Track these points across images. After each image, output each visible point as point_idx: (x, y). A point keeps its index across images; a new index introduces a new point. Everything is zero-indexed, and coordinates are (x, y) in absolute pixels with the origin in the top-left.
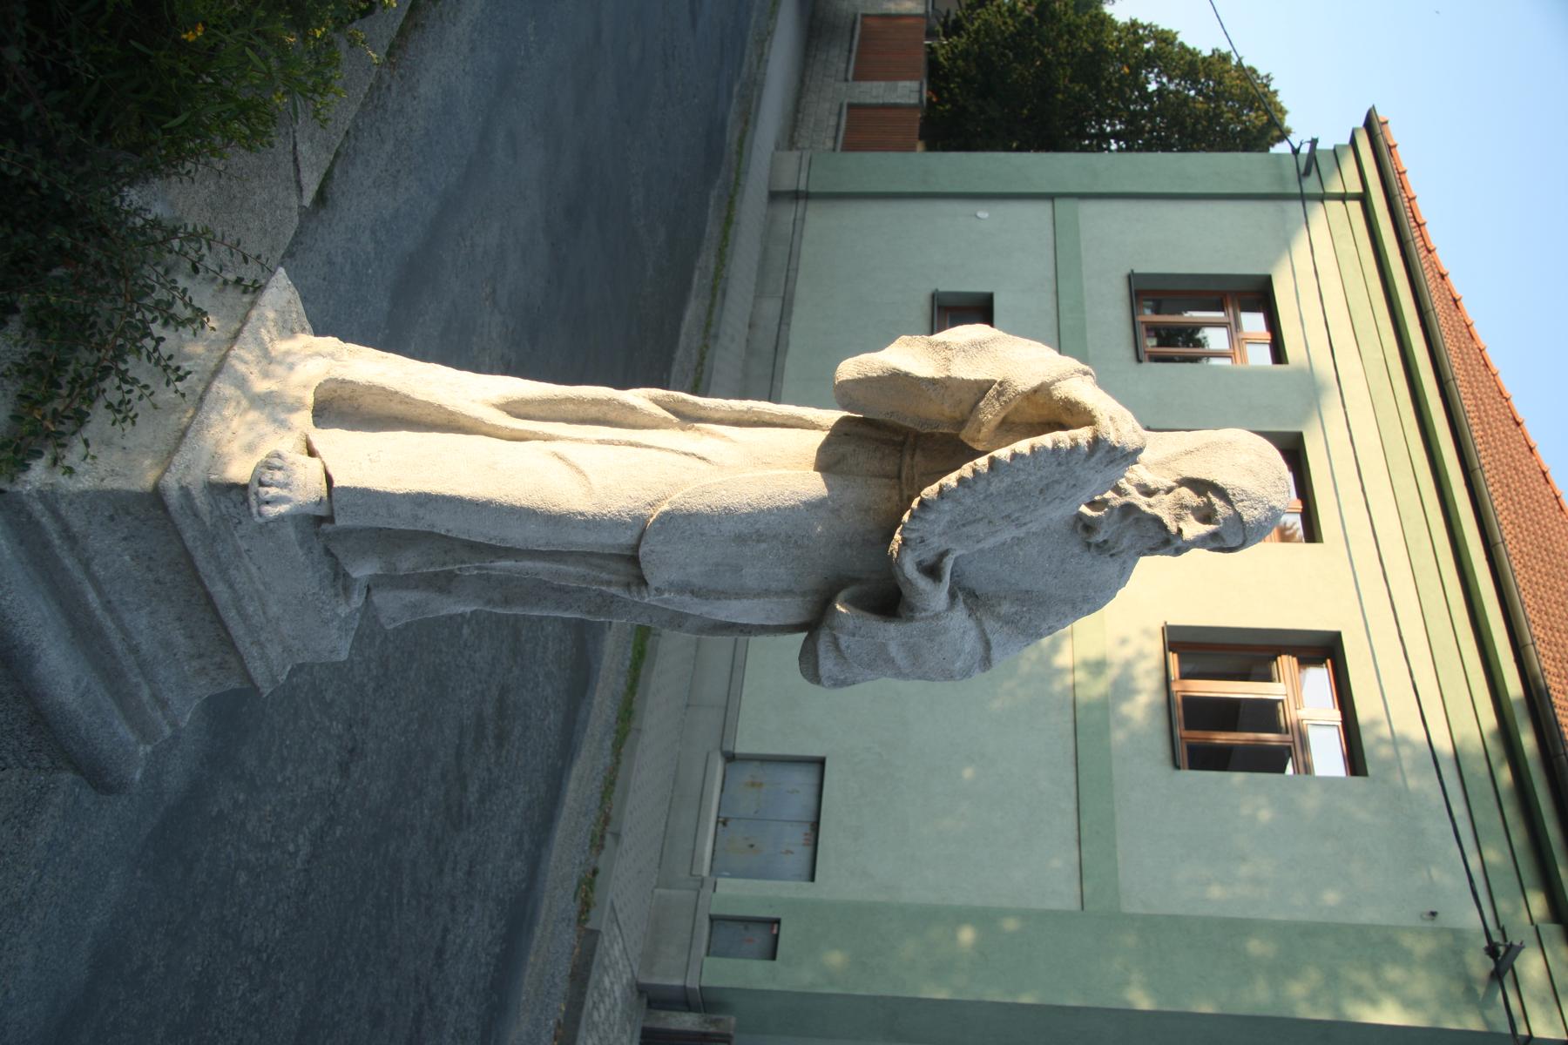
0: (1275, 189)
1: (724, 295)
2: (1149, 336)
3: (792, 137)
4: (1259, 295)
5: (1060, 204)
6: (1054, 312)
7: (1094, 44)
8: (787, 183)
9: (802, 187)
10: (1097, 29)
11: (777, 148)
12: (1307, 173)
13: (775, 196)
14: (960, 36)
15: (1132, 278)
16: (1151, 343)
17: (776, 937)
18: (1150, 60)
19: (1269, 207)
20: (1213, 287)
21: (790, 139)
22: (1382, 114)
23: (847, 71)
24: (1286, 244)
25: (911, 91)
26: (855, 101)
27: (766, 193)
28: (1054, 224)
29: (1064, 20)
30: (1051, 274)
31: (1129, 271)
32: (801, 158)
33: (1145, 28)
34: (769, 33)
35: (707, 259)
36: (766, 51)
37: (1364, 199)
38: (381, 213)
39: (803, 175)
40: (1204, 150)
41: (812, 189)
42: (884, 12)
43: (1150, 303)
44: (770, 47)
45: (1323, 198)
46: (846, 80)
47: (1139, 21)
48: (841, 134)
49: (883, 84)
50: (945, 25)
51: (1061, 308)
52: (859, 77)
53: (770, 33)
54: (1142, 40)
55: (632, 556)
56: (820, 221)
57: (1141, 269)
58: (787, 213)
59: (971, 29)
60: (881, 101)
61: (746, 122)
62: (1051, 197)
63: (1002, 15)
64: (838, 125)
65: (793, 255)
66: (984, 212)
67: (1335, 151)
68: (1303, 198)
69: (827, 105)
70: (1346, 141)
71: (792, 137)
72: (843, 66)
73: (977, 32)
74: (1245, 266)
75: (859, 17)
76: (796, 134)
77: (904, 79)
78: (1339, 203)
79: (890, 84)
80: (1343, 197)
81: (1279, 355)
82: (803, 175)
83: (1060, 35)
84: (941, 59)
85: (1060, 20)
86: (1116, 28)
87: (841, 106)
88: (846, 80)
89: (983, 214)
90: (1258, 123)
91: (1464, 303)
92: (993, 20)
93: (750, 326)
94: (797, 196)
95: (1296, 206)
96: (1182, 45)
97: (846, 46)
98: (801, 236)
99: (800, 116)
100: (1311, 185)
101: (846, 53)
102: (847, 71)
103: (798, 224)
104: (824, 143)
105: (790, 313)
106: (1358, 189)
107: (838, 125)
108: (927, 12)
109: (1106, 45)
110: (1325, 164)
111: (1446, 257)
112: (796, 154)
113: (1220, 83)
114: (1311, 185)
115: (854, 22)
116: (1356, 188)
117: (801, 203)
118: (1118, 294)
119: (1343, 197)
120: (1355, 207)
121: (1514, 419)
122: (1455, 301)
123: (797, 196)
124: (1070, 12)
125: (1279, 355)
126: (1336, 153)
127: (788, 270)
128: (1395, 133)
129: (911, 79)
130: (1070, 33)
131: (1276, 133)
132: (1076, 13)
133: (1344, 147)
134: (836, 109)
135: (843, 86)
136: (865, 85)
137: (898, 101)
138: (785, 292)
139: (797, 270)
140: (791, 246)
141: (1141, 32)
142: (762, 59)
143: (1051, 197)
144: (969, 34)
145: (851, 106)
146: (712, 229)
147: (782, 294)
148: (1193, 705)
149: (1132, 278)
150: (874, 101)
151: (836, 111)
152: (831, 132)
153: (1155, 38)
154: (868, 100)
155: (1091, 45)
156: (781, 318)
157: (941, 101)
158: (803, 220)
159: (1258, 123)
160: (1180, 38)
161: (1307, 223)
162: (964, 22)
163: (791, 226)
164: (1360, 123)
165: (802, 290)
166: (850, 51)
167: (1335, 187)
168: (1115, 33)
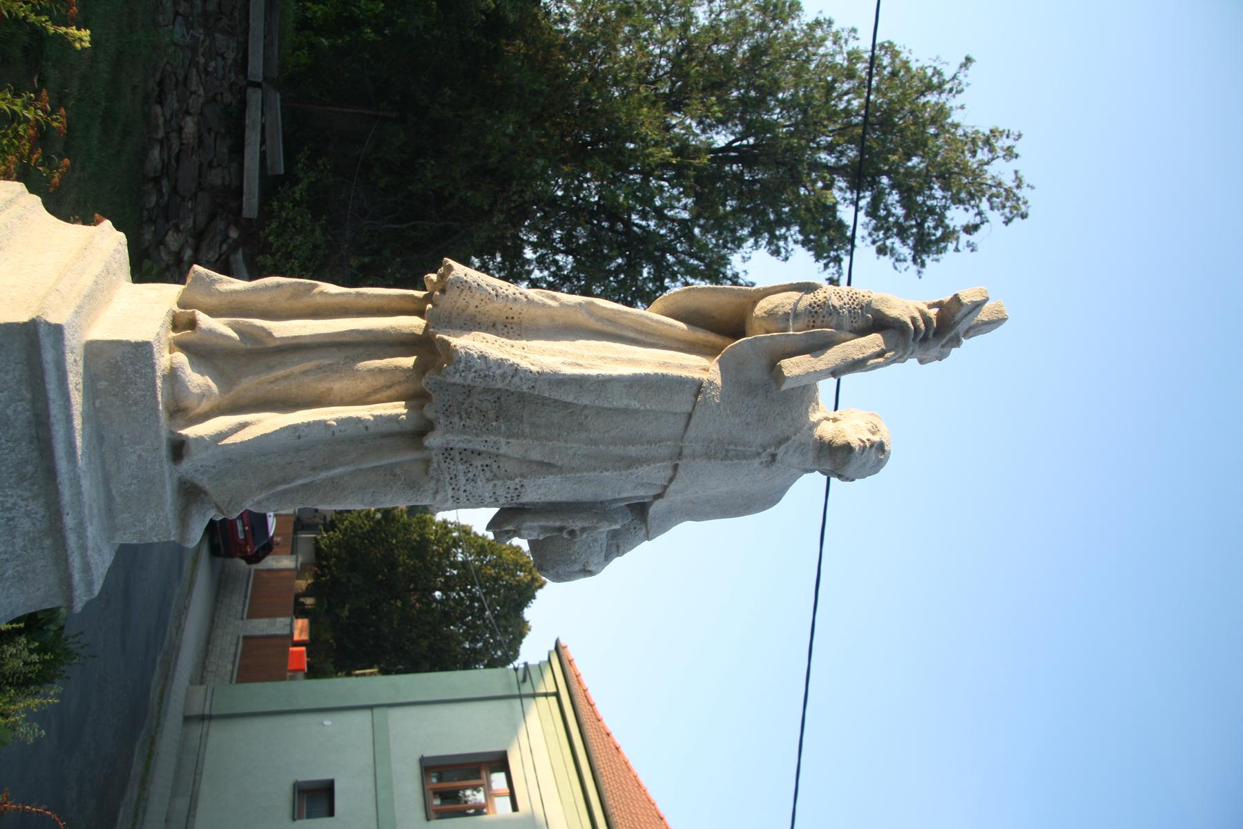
0: (507, 693)
1: (144, 812)
2: (435, 798)
3: (204, 663)
4: (500, 762)
5: (376, 711)
6: (373, 789)
7: (420, 535)
8: (196, 710)
9: (207, 712)
10: (422, 525)
11: (192, 683)
12: (524, 680)
13: (188, 719)
14: (335, 532)
15: (423, 760)
16: (437, 802)
18: (456, 543)
19: (504, 703)
20: (473, 760)
21: (201, 675)
22: (563, 642)
23: (243, 611)
24: (514, 731)
25: (285, 625)
26: (247, 634)
27: (181, 719)
28: (373, 726)
29: (401, 520)
30: (371, 762)
31: (419, 756)
32: (207, 690)
33: (452, 524)
34: (185, 608)
35: (132, 792)
36: (183, 623)
37: (557, 694)
38: (9, 167)
39: (208, 703)
40: (460, 669)
41: (214, 713)
42: (269, 567)
43: (436, 774)
44: (186, 618)
45: (534, 696)
46: (242, 619)
47: (448, 520)
48: (238, 660)
49: (266, 620)
50: (324, 525)
51: (378, 786)
52: (252, 615)
53: (186, 608)
54: (450, 531)
55: (230, 555)
56: (219, 734)
57: (428, 754)
58: (196, 730)
59: (342, 527)
60: (265, 633)
61: (166, 678)
62: (370, 707)
63: (361, 518)
64: (236, 653)
65: (199, 762)
66: (328, 721)
67: (539, 665)
68: (521, 697)
69: (229, 638)
70: (546, 659)
71: (204, 663)
72: (240, 608)
73: (346, 529)
74: (487, 745)
75: (252, 572)
76: (207, 661)
77: (280, 616)
78: (544, 698)
79: (272, 620)
80: (546, 695)
81: (515, 807)
82: (208, 703)
83: (398, 530)
84: (323, 547)
85: (398, 521)
86: (434, 524)
87: (238, 637)
88: (242, 619)
89: (327, 723)
90: (526, 580)
91: (623, 749)
92: (356, 522)
93: (167, 821)
94: (203, 718)
95: (517, 702)
96: (475, 534)
97: (243, 593)
98: (205, 748)
99: (210, 647)
100: (527, 689)
101: (243, 599)
102: (243, 611)
103: (204, 738)
104: (226, 667)
105: (196, 807)
106: (554, 690)
107: (236, 653)
108: (297, 567)
109: (427, 536)
110: (535, 674)
111: (610, 723)
112: (203, 687)
113: (500, 557)
114: (527, 689)
115: (249, 576)
116: (552, 689)
117: (206, 723)
118: (414, 770)
119: (546, 695)
120: (553, 699)
121: (659, 816)
122: (617, 749)
123: (203, 718)
124: (405, 516)
125: (515, 807)
126: (540, 667)
127: (195, 774)
128: (573, 652)
129: (285, 615)
130: (405, 529)
131: (537, 584)
132: (408, 516)
133: (544, 662)
134: (235, 641)
135: (240, 623)
136: (255, 622)
137: (277, 632)
138: (192, 792)
139: (201, 773)
140: (198, 755)
141: (449, 526)
142: (180, 629)
143: (370, 707)
144: (340, 531)
145: (245, 638)
146: (137, 768)
147: (190, 793)
149: (423, 760)
150: (260, 633)
151: (235, 642)
152: (231, 658)
153: (459, 530)
154: (257, 633)
155: (418, 536)
156: (189, 812)
157: (323, 575)
158: (207, 735)
159: (526, 580)
160: (474, 529)
161: (524, 717)
162: (337, 522)
163: (199, 740)
164: (553, 648)
165: (205, 789)
166: (246, 597)
167: (542, 690)
168: (434, 528)
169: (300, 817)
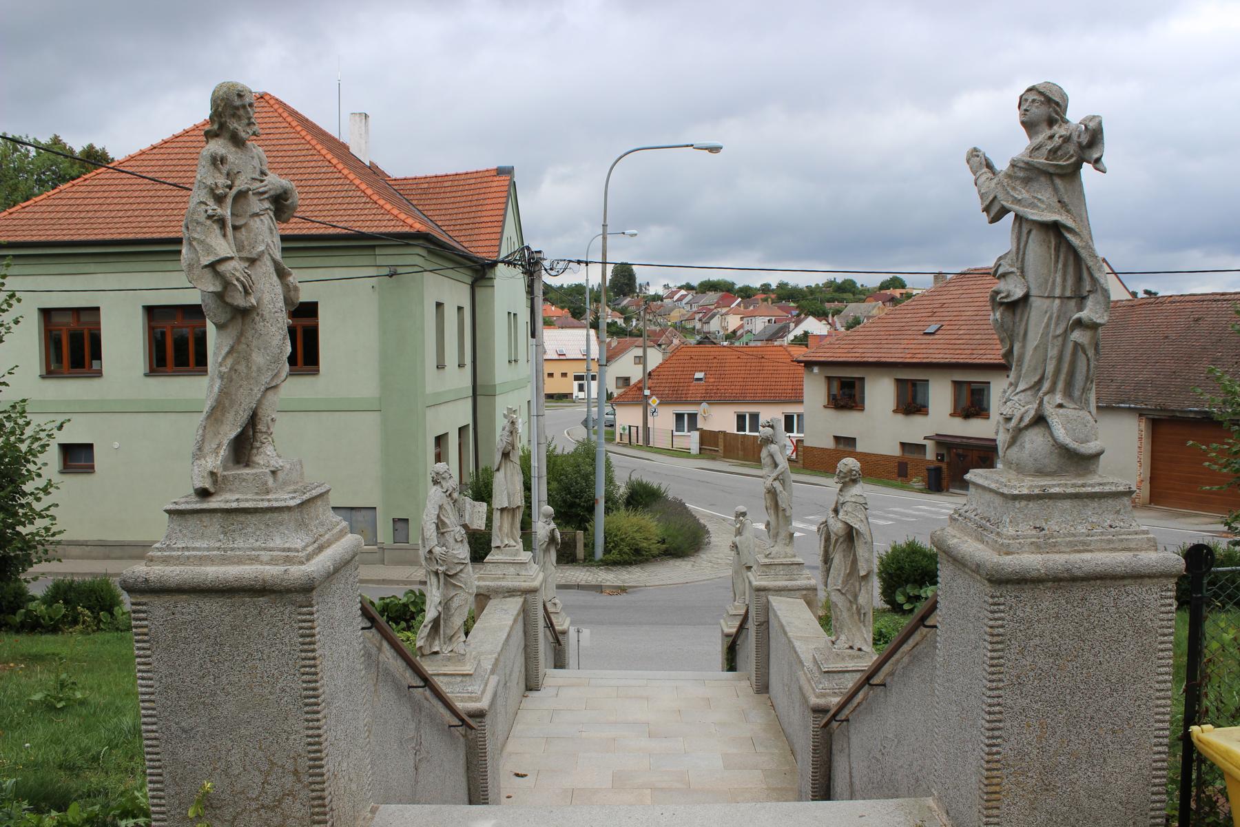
17: (399, 519)
148: (744, 417)
169: (93, 467)
